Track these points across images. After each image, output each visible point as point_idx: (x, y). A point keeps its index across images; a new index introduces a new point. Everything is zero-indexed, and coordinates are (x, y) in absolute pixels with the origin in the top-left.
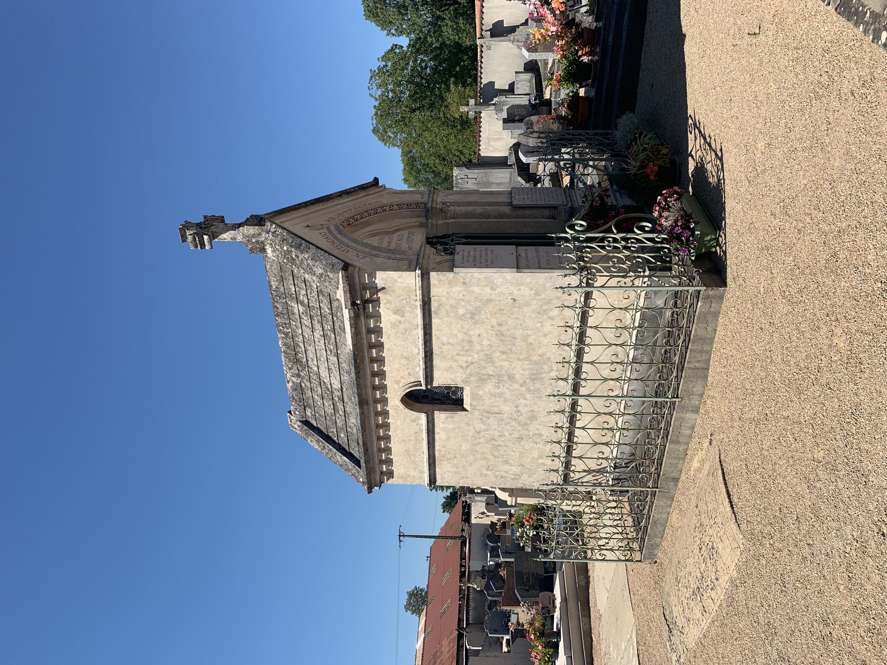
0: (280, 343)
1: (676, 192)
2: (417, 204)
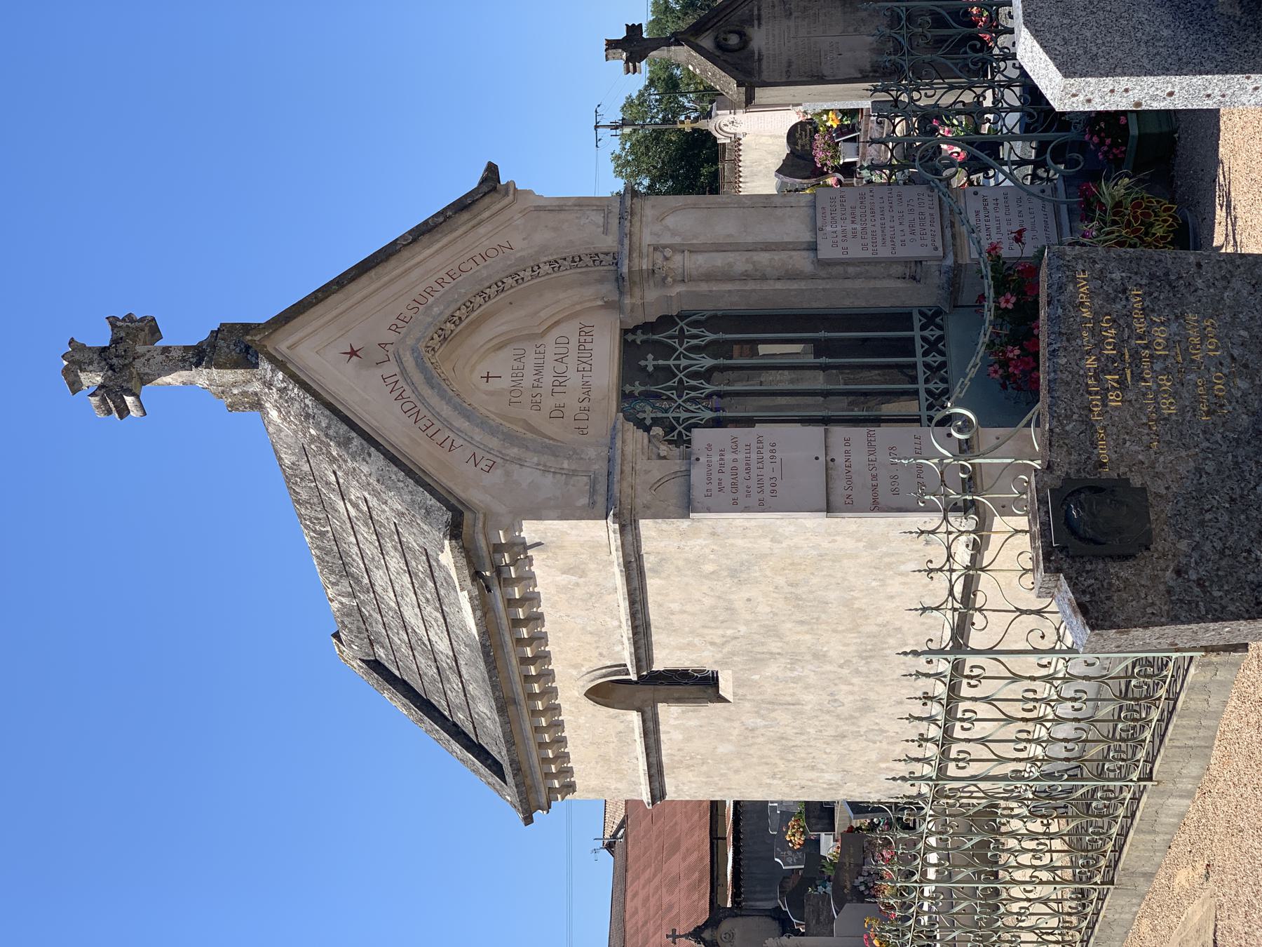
2: (595, 257)
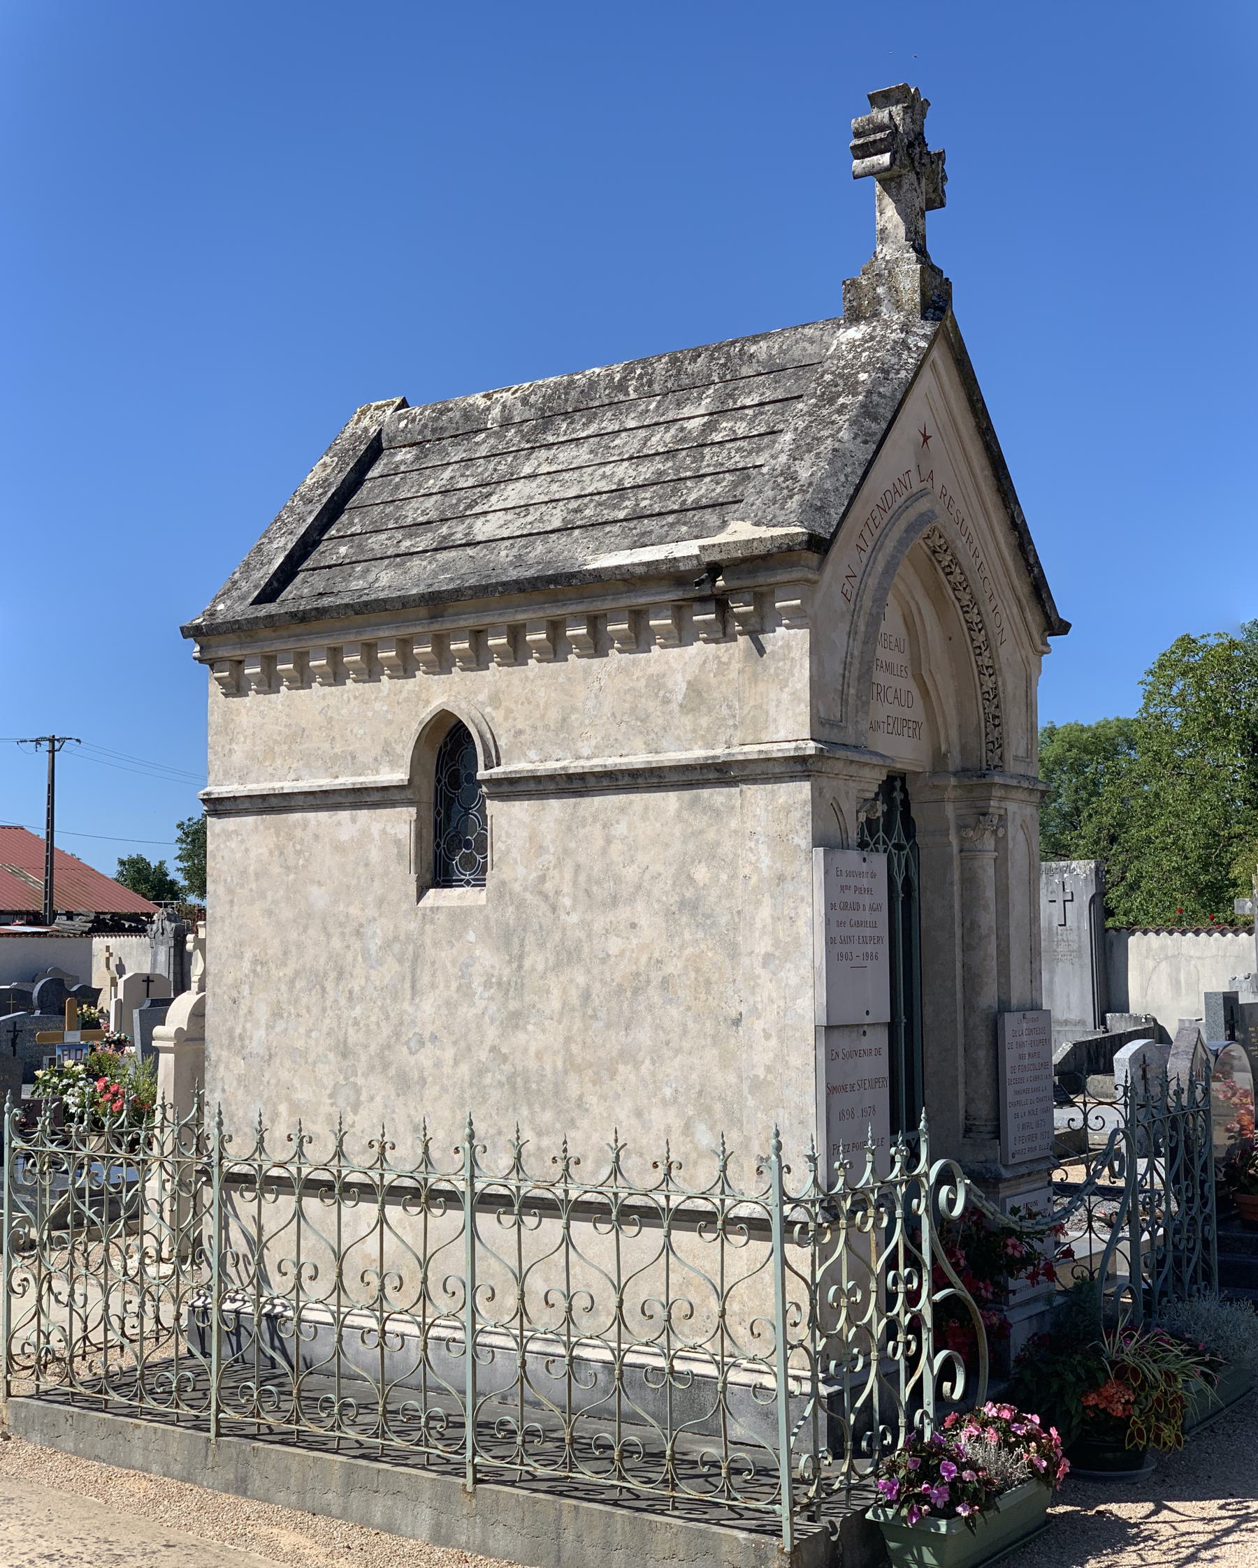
0: (597, 370)
1: (1053, 1466)
2: (997, 744)
